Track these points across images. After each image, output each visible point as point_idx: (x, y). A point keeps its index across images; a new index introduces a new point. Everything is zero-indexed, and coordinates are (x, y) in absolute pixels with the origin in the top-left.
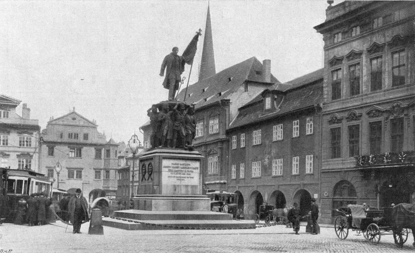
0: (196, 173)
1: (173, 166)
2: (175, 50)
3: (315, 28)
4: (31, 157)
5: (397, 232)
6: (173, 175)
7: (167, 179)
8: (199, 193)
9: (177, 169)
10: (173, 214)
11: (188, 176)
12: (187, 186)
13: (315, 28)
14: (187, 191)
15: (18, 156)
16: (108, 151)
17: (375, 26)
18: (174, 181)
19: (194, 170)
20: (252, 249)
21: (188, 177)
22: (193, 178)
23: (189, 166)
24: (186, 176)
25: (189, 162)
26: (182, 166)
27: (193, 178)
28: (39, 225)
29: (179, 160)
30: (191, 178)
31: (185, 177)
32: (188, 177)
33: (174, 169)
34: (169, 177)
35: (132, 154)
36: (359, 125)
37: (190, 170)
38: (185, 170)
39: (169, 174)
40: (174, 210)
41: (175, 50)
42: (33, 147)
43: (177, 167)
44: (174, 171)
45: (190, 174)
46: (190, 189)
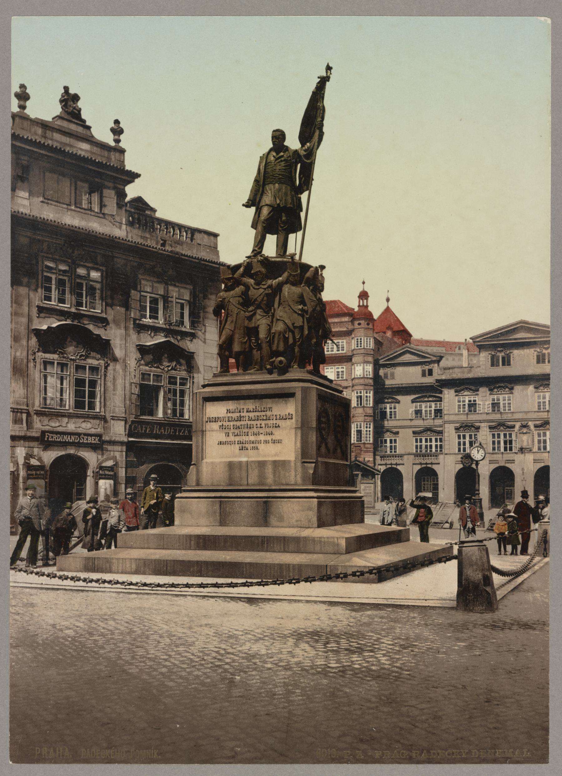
1: (229, 415)
2: (279, 137)
3: (138, 176)
4: (478, 428)
6: (232, 438)
7: (216, 453)
8: (292, 480)
9: (238, 423)
10: (157, 557)
11: (269, 438)
12: (262, 464)
13: (138, 176)
15: (457, 429)
16: (539, 409)
19: (281, 423)
20: (354, 574)
21: (266, 442)
22: (279, 442)
23: (269, 413)
24: (262, 438)
25: (268, 403)
27: (279, 442)
30: (274, 442)
31: (260, 442)
32: (266, 442)
33: (232, 423)
34: (221, 443)
37: (270, 422)
38: (258, 423)
40: (223, 523)
41: (279, 137)
44: (236, 427)
46: (269, 470)
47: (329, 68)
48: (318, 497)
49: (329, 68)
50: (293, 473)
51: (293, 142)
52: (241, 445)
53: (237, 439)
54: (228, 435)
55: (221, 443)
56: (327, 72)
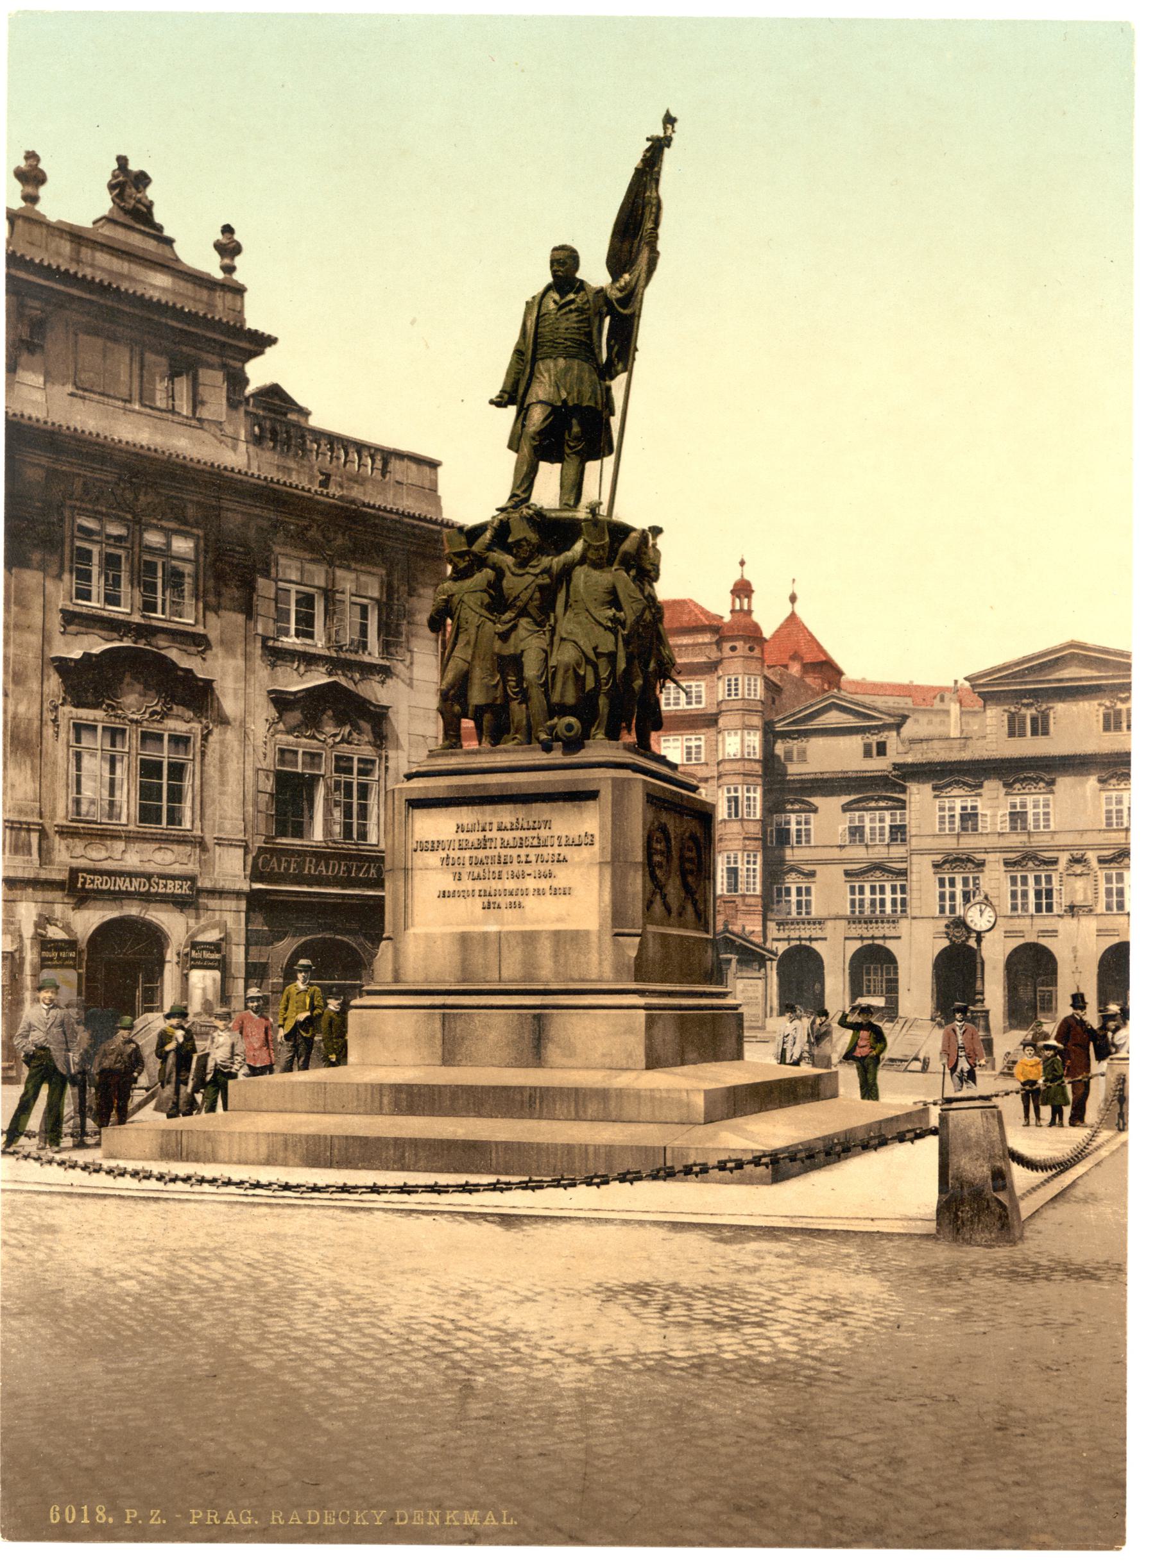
0: (581, 863)
1: (462, 836)
2: (565, 263)
5: (83, 887)
6: (467, 884)
7: (434, 914)
9: (481, 854)
11: (544, 884)
12: (529, 939)
14: (530, 965)
15: (937, 866)
17: (548, 581)
18: (467, 916)
21: (539, 892)
22: (566, 892)
23: (544, 833)
24: (531, 883)
25: (542, 810)
26: (508, 836)
27: (566, 892)
28: (242, 306)
29: (488, 808)
30: (555, 892)
31: (525, 892)
32: (539, 892)
33: (467, 854)
34: (444, 894)
35: (755, 740)
36: (320, 755)
38: (523, 852)
39: (446, 882)
41: (565, 263)
42: (413, 977)
43: (483, 844)
44: (478, 863)
45: (549, 875)
46: (545, 950)
47: (669, 120)
48: (646, 1007)
49: (669, 120)
50: (594, 957)
51: (594, 272)
52: (486, 899)
53: (479, 885)
54: (458, 877)
55: (444, 894)
56: (665, 129)
